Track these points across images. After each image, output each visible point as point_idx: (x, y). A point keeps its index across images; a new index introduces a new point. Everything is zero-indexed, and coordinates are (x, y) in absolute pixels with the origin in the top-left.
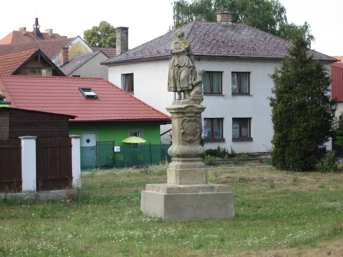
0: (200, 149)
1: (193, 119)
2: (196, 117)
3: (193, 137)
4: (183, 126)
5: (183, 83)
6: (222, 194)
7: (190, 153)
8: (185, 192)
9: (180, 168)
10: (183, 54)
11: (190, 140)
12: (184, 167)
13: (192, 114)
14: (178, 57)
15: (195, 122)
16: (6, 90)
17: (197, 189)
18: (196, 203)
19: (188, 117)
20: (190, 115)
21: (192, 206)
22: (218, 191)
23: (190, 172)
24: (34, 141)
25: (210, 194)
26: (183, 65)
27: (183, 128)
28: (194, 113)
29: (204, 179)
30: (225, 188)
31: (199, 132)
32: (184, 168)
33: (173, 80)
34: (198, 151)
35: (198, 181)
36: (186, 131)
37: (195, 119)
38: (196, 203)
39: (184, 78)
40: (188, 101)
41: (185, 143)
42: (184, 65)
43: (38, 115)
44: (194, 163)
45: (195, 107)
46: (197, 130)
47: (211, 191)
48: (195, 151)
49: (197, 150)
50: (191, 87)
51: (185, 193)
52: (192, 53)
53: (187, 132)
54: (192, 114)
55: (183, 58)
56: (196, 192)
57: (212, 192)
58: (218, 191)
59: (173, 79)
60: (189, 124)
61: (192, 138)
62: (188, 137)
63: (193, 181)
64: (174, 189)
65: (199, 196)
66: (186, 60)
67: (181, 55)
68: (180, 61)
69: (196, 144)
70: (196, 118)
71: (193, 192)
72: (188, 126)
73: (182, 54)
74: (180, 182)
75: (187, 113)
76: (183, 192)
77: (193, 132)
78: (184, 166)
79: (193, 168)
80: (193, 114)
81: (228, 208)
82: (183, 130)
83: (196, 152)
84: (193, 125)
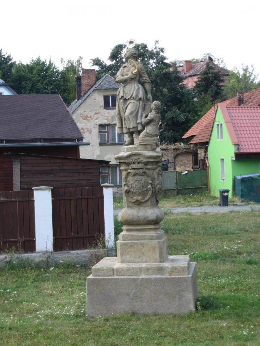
0: (151, 214)
1: (140, 171)
2: (146, 169)
4: (127, 182)
5: (129, 122)
6: (173, 278)
7: (136, 219)
8: (121, 274)
9: (123, 240)
10: (132, 82)
11: (137, 201)
12: (128, 239)
13: (140, 165)
14: (124, 87)
15: (145, 176)
16: (230, 121)
17: (138, 270)
18: (134, 291)
20: (136, 166)
21: (129, 295)
22: (170, 275)
23: (135, 246)
24: (49, 192)
25: (155, 278)
26: (129, 97)
27: (128, 185)
28: (142, 163)
29: (157, 256)
30: (181, 270)
31: (150, 190)
32: (129, 240)
33: (119, 118)
35: (148, 259)
36: (131, 188)
37: (144, 172)
38: (134, 291)
39: (128, 115)
40: (135, 147)
41: (132, 205)
44: (144, 233)
46: (147, 187)
47: (159, 273)
48: (144, 216)
49: (146, 215)
50: (140, 128)
51: (120, 276)
52: (146, 79)
54: (140, 165)
55: (130, 88)
56: (136, 275)
57: (162, 275)
58: (170, 275)
59: (118, 116)
60: (135, 179)
61: (139, 198)
62: (134, 196)
63: (141, 258)
64: (103, 270)
65: (139, 281)
67: (130, 83)
68: (126, 92)
69: (147, 206)
70: (145, 170)
71: (131, 274)
72: (133, 182)
73: (130, 82)
74: (121, 259)
75: (131, 164)
76: (117, 275)
78: (127, 237)
80: (140, 165)
81: (183, 299)
82: (128, 186)
83: (144, 219)
84: (141, 180)
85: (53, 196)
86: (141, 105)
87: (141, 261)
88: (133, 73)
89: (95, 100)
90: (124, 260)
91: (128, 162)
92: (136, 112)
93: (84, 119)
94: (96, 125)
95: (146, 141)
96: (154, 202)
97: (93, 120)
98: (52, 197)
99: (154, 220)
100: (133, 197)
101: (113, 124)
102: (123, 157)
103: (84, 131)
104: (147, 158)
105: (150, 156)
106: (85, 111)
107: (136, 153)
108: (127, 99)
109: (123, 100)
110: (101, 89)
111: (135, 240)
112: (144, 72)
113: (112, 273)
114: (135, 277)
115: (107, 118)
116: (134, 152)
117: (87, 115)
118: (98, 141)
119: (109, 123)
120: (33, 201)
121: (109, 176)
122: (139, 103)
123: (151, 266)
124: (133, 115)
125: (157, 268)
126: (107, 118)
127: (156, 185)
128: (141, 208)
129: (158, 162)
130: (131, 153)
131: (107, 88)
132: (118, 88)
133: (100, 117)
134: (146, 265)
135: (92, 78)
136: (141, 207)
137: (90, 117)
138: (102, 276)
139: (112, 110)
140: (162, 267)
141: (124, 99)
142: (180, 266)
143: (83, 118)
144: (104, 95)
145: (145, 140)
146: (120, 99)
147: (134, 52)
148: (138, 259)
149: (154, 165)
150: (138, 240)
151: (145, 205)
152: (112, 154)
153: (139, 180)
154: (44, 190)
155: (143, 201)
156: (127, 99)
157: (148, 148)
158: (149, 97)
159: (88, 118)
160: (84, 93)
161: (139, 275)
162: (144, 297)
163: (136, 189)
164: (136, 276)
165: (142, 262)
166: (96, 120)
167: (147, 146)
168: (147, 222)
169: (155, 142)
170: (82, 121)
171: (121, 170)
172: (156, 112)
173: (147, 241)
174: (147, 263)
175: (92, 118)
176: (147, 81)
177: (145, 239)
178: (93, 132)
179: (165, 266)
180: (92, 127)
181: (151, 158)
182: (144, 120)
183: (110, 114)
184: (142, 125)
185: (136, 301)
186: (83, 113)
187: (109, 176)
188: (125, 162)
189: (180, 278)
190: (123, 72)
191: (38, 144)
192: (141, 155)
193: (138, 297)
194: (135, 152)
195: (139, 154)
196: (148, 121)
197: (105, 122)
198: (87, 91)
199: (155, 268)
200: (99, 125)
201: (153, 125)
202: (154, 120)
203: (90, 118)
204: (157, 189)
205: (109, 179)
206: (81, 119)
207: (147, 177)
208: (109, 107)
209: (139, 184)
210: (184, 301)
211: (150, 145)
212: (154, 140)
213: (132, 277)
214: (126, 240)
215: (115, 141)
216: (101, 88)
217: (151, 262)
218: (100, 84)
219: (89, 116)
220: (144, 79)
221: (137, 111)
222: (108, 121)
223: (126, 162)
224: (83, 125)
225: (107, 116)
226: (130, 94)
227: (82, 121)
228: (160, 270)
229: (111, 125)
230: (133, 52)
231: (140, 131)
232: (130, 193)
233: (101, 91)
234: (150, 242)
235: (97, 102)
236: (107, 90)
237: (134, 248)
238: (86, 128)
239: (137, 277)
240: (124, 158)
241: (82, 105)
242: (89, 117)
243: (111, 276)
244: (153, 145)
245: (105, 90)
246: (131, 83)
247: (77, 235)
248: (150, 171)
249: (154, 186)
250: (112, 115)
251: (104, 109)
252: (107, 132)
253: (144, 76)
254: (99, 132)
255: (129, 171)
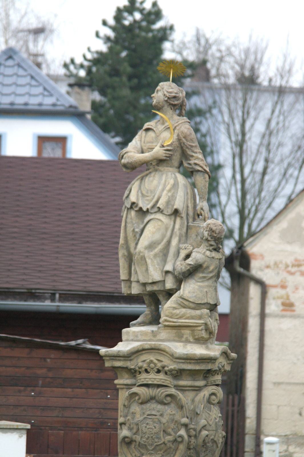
19: (147, 386)
20: (152, 378)
24: (20, 437)
28: (166, 373)
42: (153, 207)
43: (52, 356)
53: (138, 438)
54: (159, 380)
66: (163, 190)
73: (156, 167)
77: (159, 438)
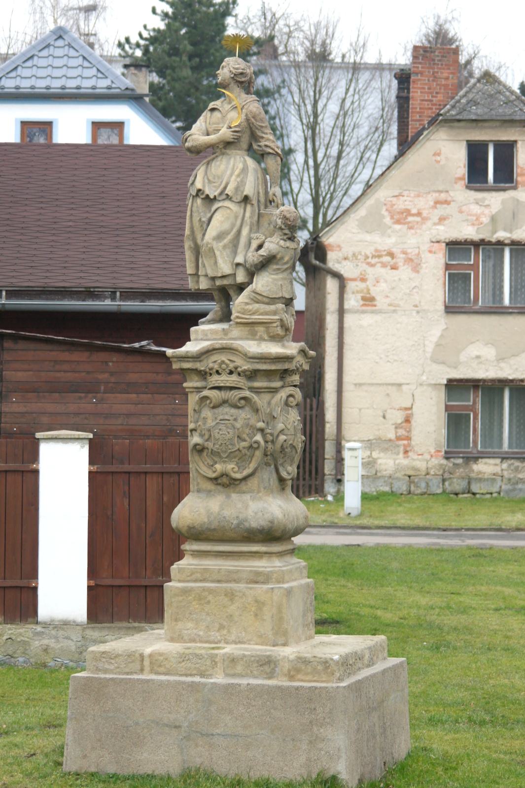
1: (234, 395)
2: (251, 389)
3: (237, 464)
8: (162, 669)
12: (194, 577)
13: (233, 380)
15: (247, 409)
17: (208, 663)
19: (219, 388)
24: (82, 447)
25: (248, 684)
26: (216, 193)
28: (239, 374)
32: (196, 581)
34: (246, 520)
40: (224, 329)
42: (221, 194)
45: (240, 352)
46: (251, 438)
49: (241, 516)
52: (266, 146)
53: (210, 445)
54: (233, 380)
56: (202, 675)
62: (216, 463)
64: (117, 656)
66: (231, 175)
67: (223, 154)
70: (247, 393)
73: (223, 150)
75: (211, 374)
76: (152, 671)
79: (227, 581)
80: (234, 377)
83: (238, 525)
84: (235, 420)
85: (93, 459)
86: (248, 214)
87: (225, 639)
88: (230, 127)
89: (438, 158)
90: (179, 635)
91: (202, 369)
92: (232, 233)
93: (398, 222)
94: (438, 242)
95: (254, 314)
96: (269, 480)
97: (429, 224)
98: (92, 461)
99: (263, 529)
100: (212, 466)
101: (494, 240)
102: (190, 355)
103: (394, 261)
104: (252, 360)
105: (259, 356)
106: (401, 195)
107: (224, 346)
108: (212, 197)
109: (202, 199)
110: (459, 121)
111: (213, 581)
112: (262, 127)
113: (139, 667)
114: (197, 679)
115: (474, 218)
116: (220, 342)
117: (409, 207)
118: (441, 298)
119: (481, 236)
120: (36, 472)
121: (475, 418)
122: (242, 211)
123: (242, 652)
124: (226, 241)
125: (257, 659)
126: (477, 219)
127: (275, 435)
128: (234, 496)
129: (285, 373)
130: (211, 345)
131: (480, 118)
132: (193, 167)
133: (452, 216)
134: (236, 649)
135: (447, 78)
136: (234, 492)
137: (419, 214)
138: (113, 673)
139: (494, 194)
140: (269, 656)
141: (203, 196)
142: (319, 656)
143: (392, 218)
144: (467, 141)
145: (250, 311)
146: (195, 199)
147: (240, 71)
148: (217, 634)
149: (275, 381)
150: (219, 581)
151: (243, 486)
152: (487, 344)
153: (229, 420)
154: (66, 443)
155: (238, 476)
156: (212, 197)
157: (259, 334)
158: (274, 195)
159: (410, 219)
160: (416, 131)
161: (210, 676)
162: (218, 734)
163: (219, 443)
164: (201, 677)
165: (227, 643)
166: (438, 227)
167: (256, 329)
168: (245, 534)
169: (277, 317)
170: (390, 227)
171: (187, 390)
172: (285, 237)
173: (242, 586)
174: (239, 646)
175: (424, 219)
176: (271, 151)
177: (236, 581)
178: (424, 266)
179: (279, 655)
180: (426, 247)
181: (263, 361)
182: (253, 257)
183: (488, 206)
184: (247, 270)
185: (197, 745)
186: (395, 199)
187: (475, 418)
188: (194, 368)
189: (316, 688)
190: (208, 122)
191: (107, 304)
192: (237, 350)
193: (201, 734)
194: (221, 344)
195: (230, 349)
196: (261, 259)
197: (469, 232)
198: (426, 122)
199: (253, 659)
200: (447, 244)
201: (274, 270)
202: (278, 256)
203: (418, 219)
204: (278, 446)
205: (475, 430)
206: (388, 220)
207: (254, 411)
208: (486, 181)
209: (229, 430)
210: (323, 753)
211: (265, 325)
212: (275, 313)
213: (189, 679)
214: (188, 581)
215: (501, 299)
216: (458, 117)
217: (249, 644)
218: (458, 104)
219: (414, 211)
220: (262, 144)
221: (235, 230)
222: (478, 229)
223: (196, 370)
224: (393, 240)
225: (475, 212)
226: (220, 185)
227: (390, 227)
228: (268, 665)
229: (489, 243)
230: (237, 69)
231: (243, 286)
232: (205, 454)
233: (459, 128)
234: (251, 588)
235: (442, 163)
236: (480, 124)
237: (209, 602)
238: (405, 253)
239: (203, 680)
240: (193, 357)
241: (391, 175)
242: (413, 215)
243: (136, 673)
244: (271, 325)
245: (474, 124)
246: (228, 154)
247: (161, 578)
248: (263, 395)
249: (270, 438)
250: (494, 211)
251: (468, 191)
252: (475, 267)
253: (262, 138)
254: (448, 267)
255: (206, 393)
